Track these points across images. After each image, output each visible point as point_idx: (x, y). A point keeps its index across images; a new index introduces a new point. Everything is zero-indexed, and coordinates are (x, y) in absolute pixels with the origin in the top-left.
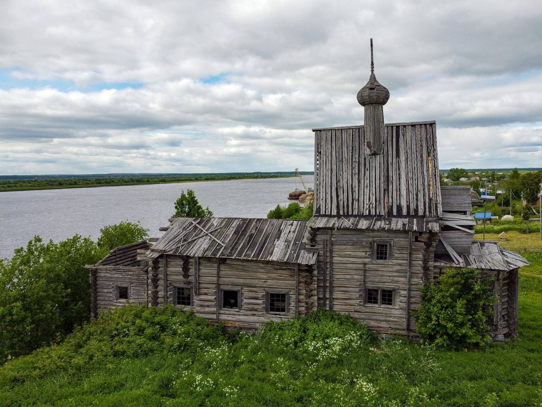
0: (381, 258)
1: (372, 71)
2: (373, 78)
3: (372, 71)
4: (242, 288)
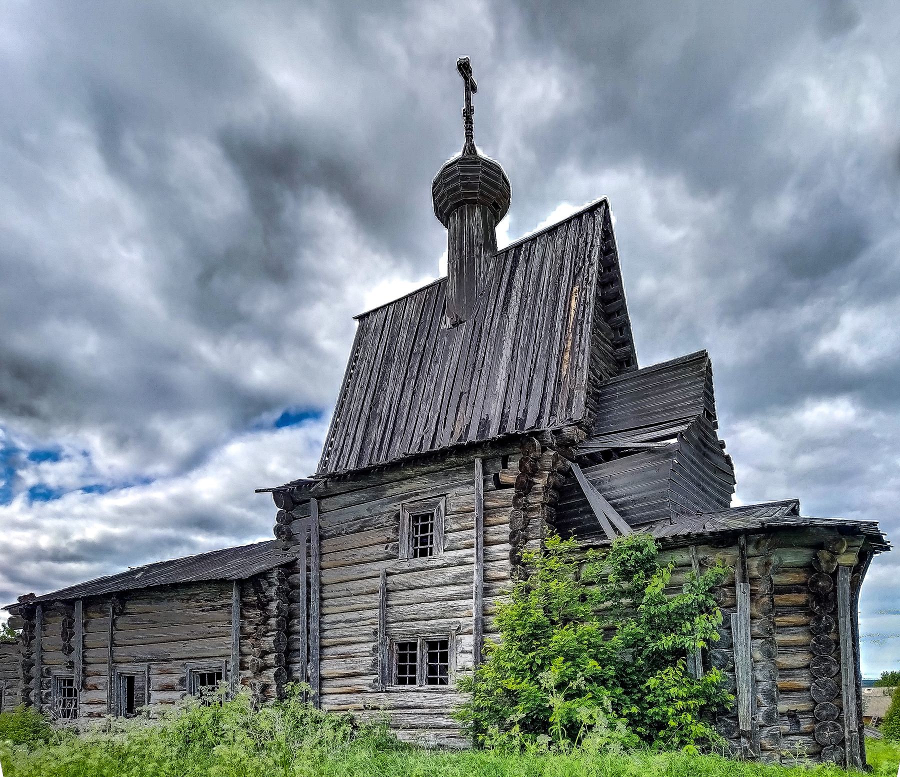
0: (423, 553)
1: (469, 136)
2: (470, 149)
3: (469, 136)
4: (149, 667)
